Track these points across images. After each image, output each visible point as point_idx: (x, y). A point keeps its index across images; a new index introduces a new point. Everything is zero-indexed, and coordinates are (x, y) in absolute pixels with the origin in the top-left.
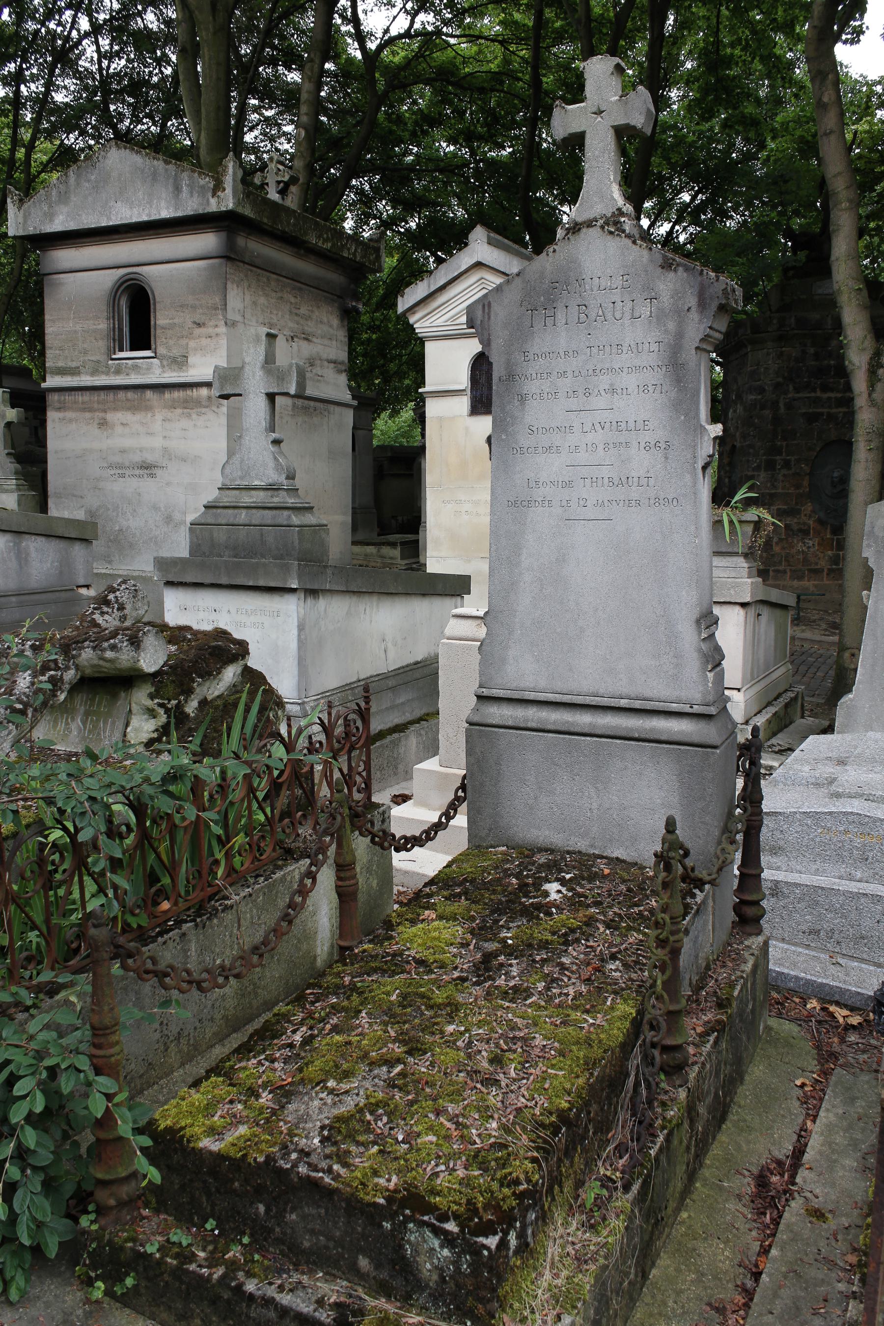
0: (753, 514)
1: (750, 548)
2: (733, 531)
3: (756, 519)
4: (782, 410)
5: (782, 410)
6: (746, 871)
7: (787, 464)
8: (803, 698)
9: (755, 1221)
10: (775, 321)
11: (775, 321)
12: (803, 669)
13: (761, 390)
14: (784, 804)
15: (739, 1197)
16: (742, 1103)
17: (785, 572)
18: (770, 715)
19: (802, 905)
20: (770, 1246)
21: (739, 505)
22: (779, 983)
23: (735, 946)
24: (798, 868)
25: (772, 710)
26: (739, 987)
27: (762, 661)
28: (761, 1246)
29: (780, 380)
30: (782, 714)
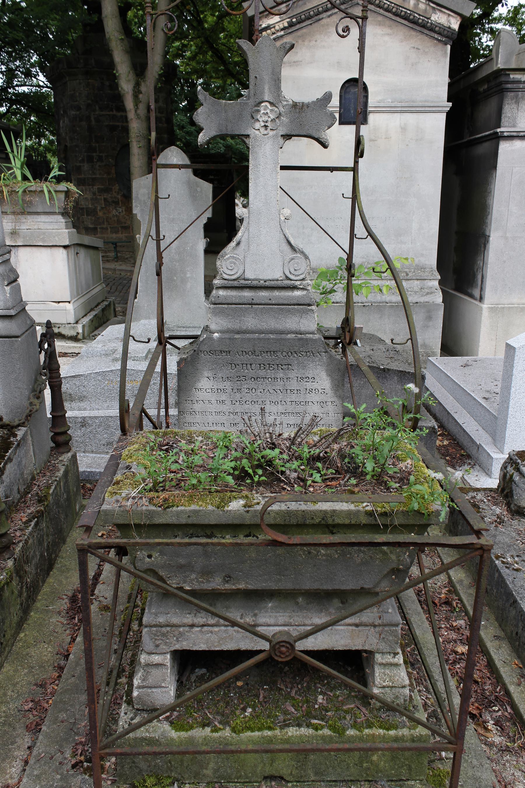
0: (63, 186)
1: (65, 209)
2: (51, 198)
3: (66, 189)
4: (93, 123)
5: (93, 123)
6: (55, 414)
7: (100, 159)
8: (114, 305)
9: (68, 624)
10: (82, 61)
11: (82, 61)
12: (120, 288)
13: (79, 108)
14: (85, 369)
15: (59, 613)
16: (64, 555)
17: (107, 229)
18: (92, 316)
19: (101, 429)
20: (77, 636)
21: (54, 180)
22: (90, 478)
23: (53, 462)
24: (97, 407)
25: (93, 313)
26: (53, 487)
27: (84, 282)
28: (72, 638)
29: (89, 101)
30: (100, 316)
